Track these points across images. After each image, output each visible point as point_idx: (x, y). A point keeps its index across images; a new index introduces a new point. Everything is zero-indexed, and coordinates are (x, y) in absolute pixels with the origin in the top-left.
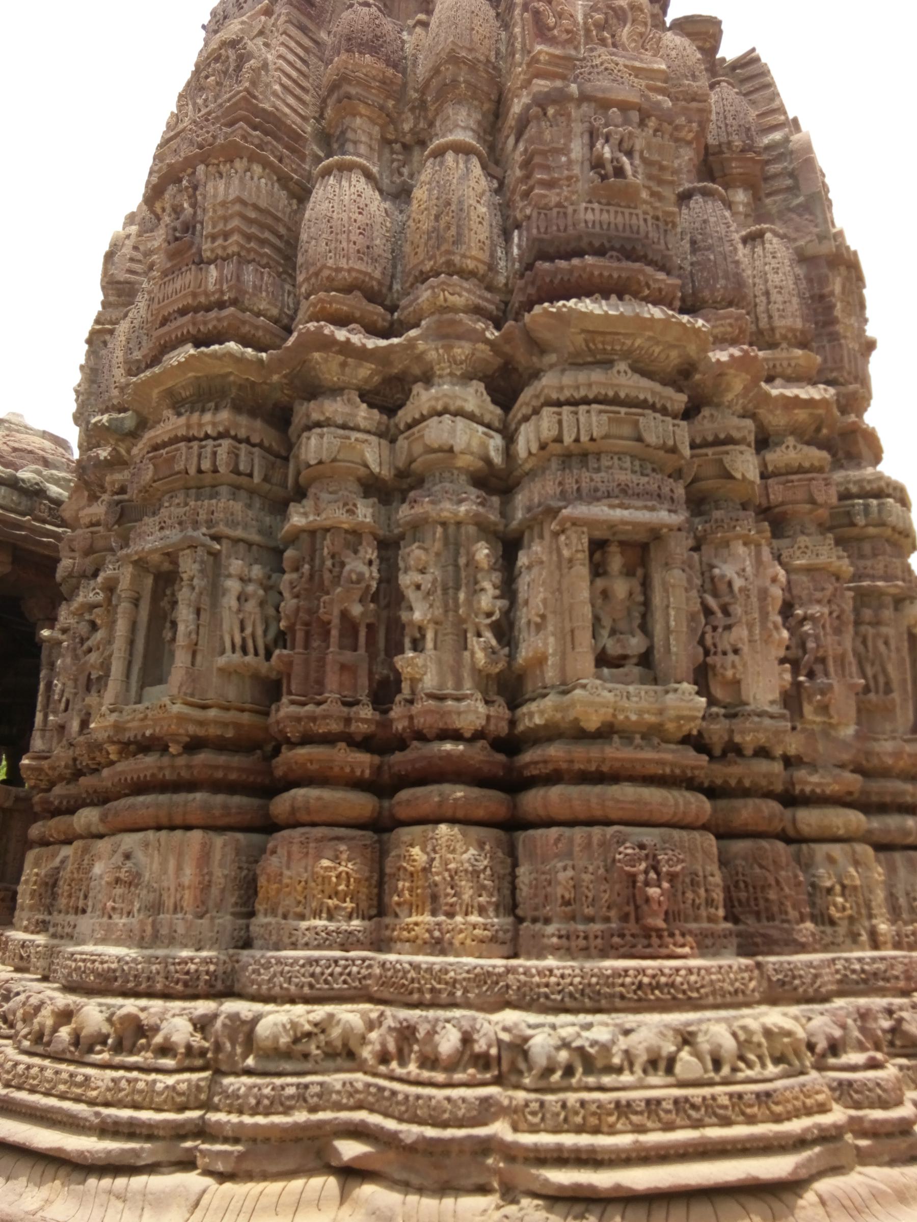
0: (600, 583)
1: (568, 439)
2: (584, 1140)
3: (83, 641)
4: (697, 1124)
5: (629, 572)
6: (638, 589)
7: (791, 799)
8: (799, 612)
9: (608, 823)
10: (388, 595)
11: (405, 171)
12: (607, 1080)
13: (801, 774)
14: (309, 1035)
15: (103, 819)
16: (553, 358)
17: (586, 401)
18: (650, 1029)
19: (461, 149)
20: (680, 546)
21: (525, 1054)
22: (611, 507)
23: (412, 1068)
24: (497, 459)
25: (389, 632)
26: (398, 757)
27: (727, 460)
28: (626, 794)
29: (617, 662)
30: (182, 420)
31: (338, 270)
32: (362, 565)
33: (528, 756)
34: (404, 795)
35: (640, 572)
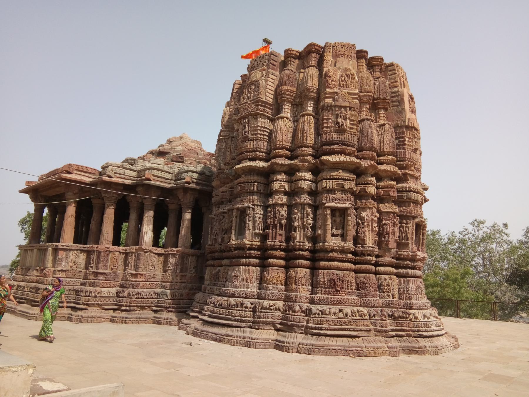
0: (334, 218)
1: (328, 188)
2: (320, 326)
3: (221, 220)
4: (341, 325)
5: (340, 216)
6: (342, 220)
7: (377, 265)
8: (384, 222)
9: (331, 270)
10: (290, 219)
11: (297, 113)
12: (325, 316)
13: (380, 259)
14: (272, 306)
15: (231, 262)
16: (326, 167)
17: (332, 179)
18: (335, 309)
19: (309, 115)
20: (352, 212)
21: (311, 311)
22: (336, 203)
23: (291, 312)
24: (314, 189)
25: (290, 228)
26: (290, 253)
27: (366, 188)
28: (335, 264)
29: (337, 236)
30: (246, 178)
31: (280, 145)
32: (284, 212)
33: (316, 255)
34: (291, 261)
35: (343, 216)
